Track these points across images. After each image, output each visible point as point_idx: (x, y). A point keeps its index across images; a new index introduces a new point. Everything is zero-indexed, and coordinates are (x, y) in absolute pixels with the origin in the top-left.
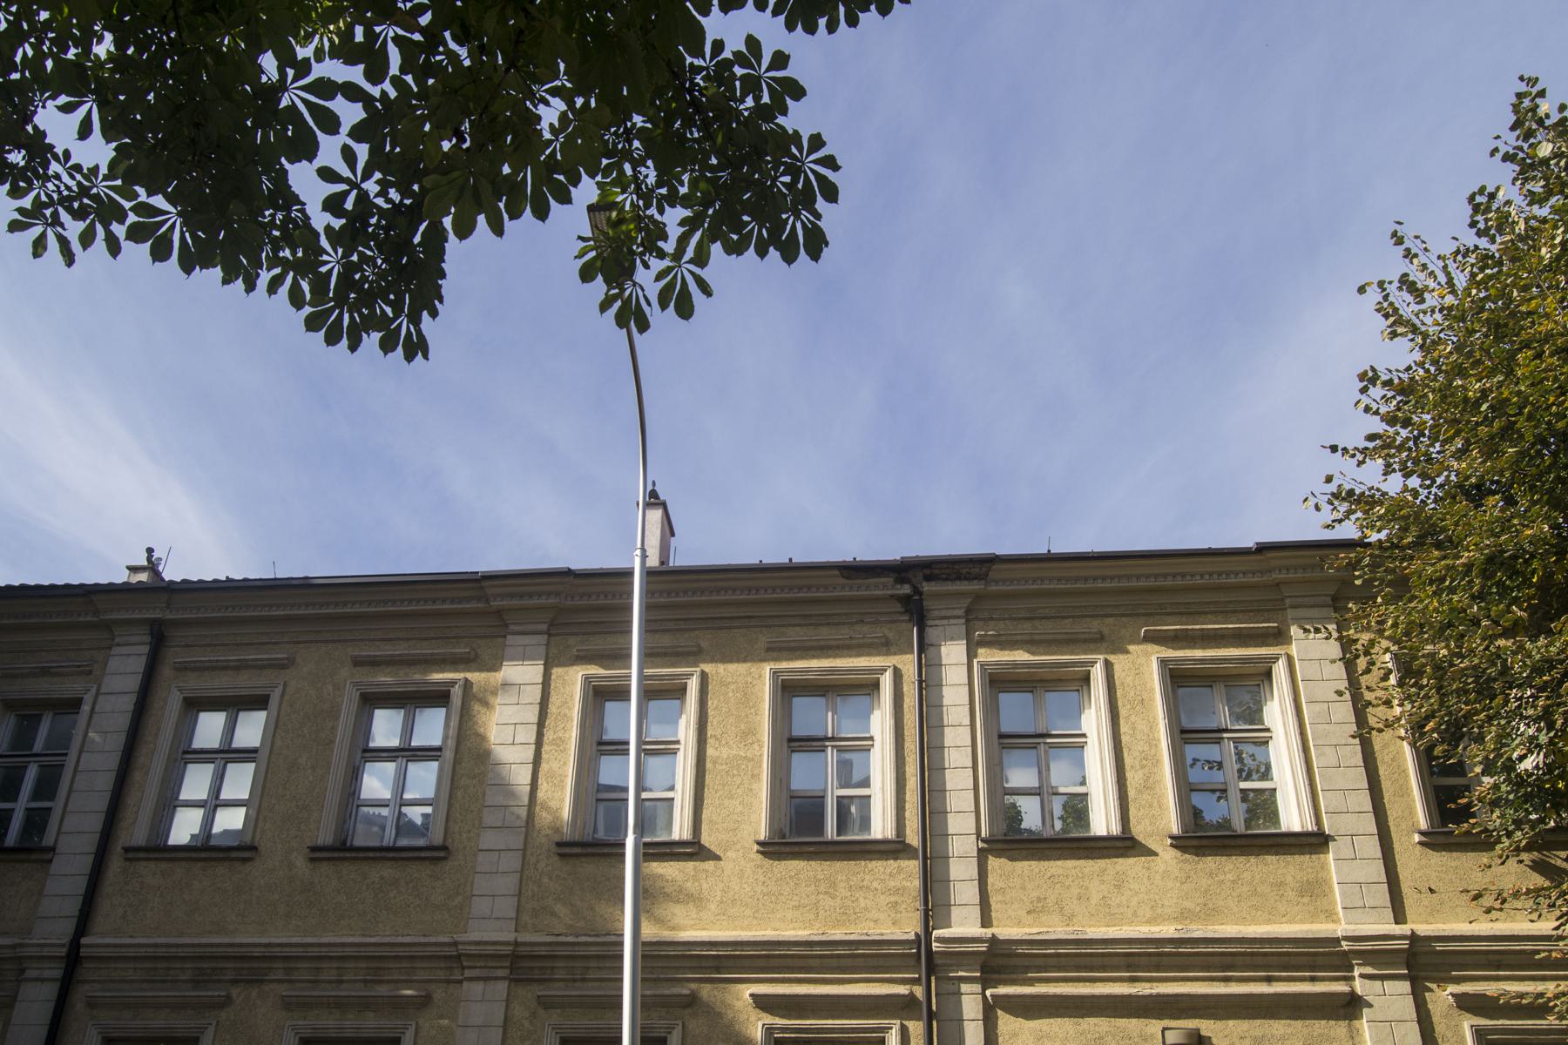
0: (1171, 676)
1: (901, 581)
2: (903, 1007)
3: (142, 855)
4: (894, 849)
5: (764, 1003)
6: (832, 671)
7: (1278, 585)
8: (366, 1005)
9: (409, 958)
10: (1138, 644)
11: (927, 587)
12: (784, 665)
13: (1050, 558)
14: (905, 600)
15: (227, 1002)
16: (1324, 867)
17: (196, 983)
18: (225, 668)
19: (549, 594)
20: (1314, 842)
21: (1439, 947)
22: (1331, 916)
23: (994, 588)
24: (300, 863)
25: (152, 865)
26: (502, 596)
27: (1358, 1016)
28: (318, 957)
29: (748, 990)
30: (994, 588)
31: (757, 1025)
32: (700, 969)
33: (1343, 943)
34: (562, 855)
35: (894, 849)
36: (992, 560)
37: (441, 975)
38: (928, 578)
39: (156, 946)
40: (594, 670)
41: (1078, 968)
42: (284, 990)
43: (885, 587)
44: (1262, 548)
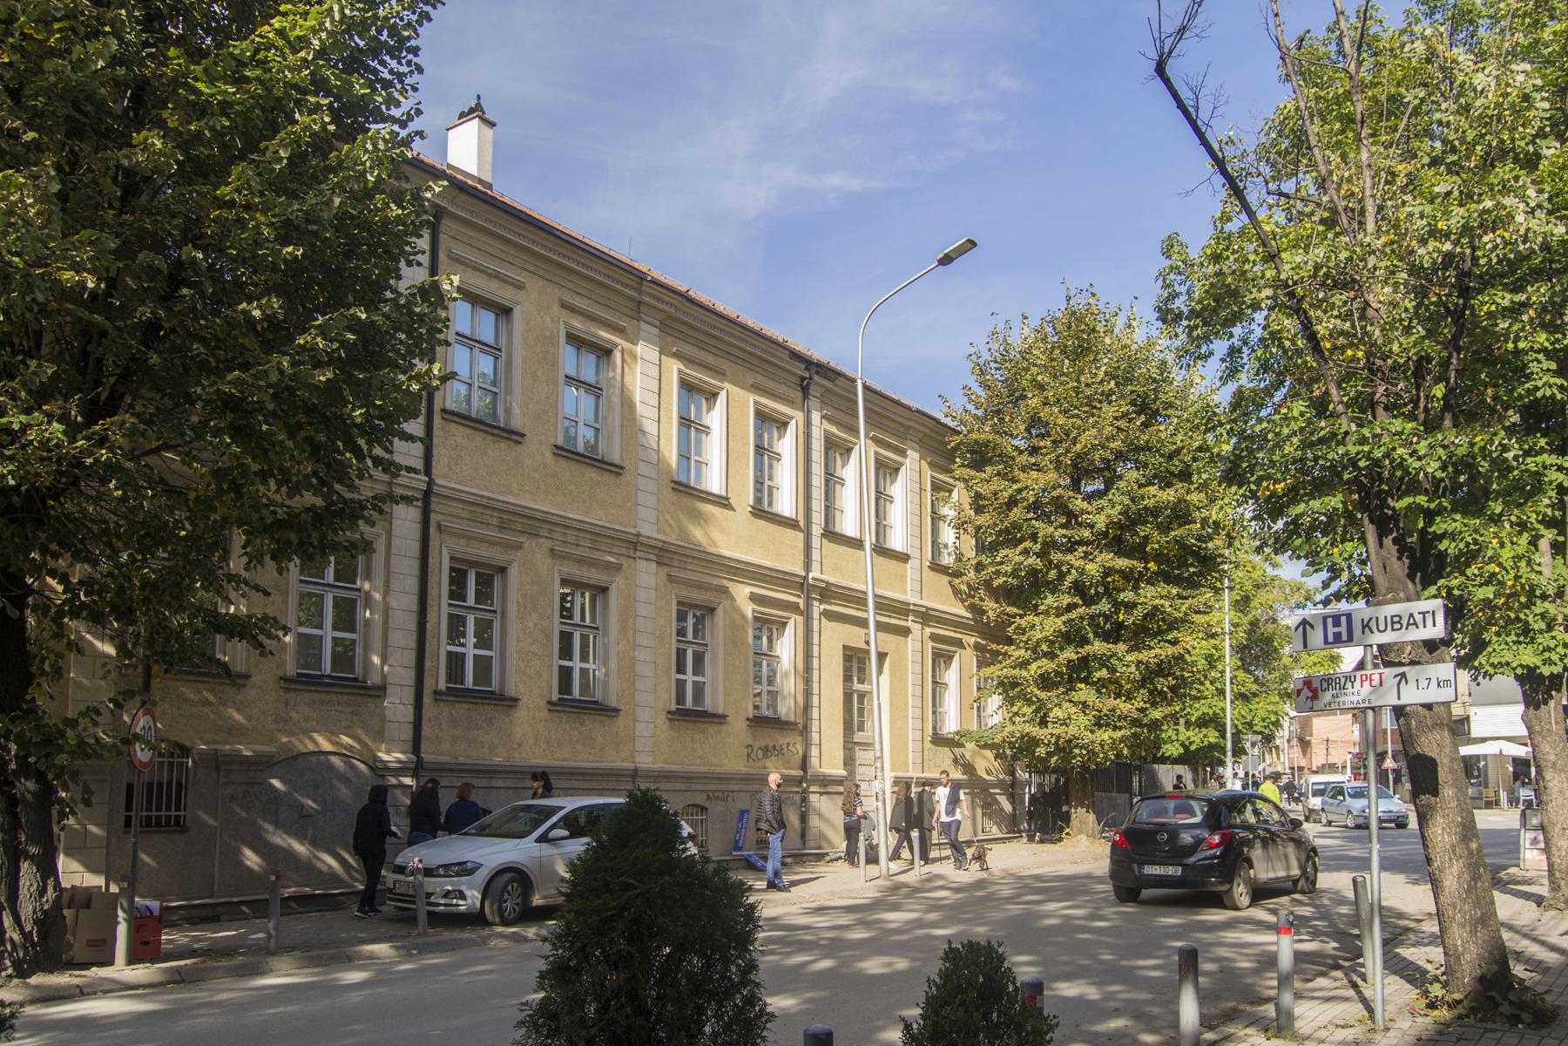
0: (826, 441)
1: (807, 369)
2: (794, 608)
3: (456, 419)
4: (791, 524)
5: (754, 598)
6: (775, 410)
7: (909, 427)
8: (593, 563)
9: (598, 535)
10: (742, 387)
11: (816, 378)
12: (941, 477)
13: (685, 297)
14: (803, 379)
15: (519, 547)
16: (906, 570)
17: (501, 528)
18: (482, 272)
19: (671, 305)
20: (903, 558)
21: (833, 589)
22: (905, 592)
23: (835, 389)
24: (548, 453)
25: (460, 427)
26: (650, 295)
27: (907, 636)
28: (579, 528)
29: (748, 590)
30: (835, 389)
31: (749, 609)
32: (727, 573)
33: (495, 522)
34: (555, 454)
35: (791, 524)
36: (839, 374)
37: (624, 551)
38: (817, 373)
39: (482, 496)
40: (833, 429)
41: (760, 580)
42: (548, 543)
43: (799, 369)
44: (918, 411)
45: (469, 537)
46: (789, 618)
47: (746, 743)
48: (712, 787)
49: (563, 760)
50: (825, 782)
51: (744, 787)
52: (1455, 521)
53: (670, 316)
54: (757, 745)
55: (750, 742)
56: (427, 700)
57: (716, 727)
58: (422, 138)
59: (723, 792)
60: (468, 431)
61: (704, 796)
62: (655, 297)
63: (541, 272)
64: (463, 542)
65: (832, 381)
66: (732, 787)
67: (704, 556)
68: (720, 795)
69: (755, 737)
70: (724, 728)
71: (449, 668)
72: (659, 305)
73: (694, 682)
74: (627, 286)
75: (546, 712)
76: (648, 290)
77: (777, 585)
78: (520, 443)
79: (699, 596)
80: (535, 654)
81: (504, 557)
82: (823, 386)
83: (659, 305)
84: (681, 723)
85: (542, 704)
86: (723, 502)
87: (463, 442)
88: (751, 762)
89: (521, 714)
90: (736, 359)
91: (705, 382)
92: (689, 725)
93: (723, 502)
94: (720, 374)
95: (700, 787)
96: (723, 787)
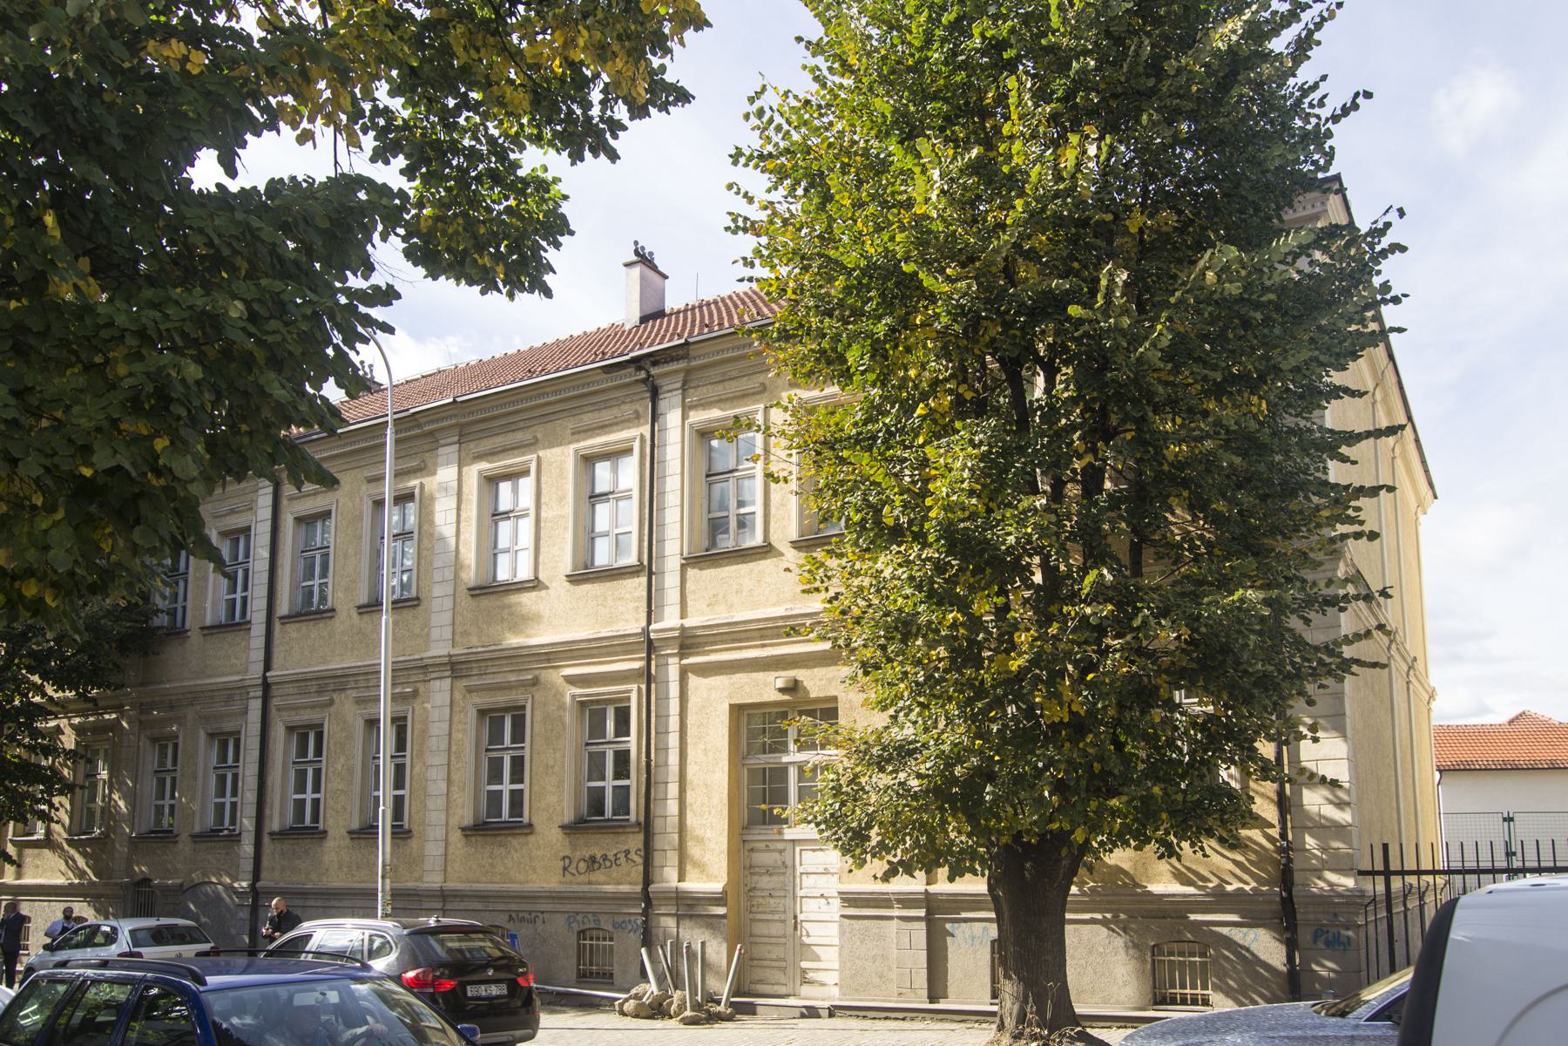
1: (639, 369)
6: (606, 444)
11: (654, 371)
14: (644, 381)
23: (694, 363)
24: (354, 613)
26: (428, 423)
30: (694, 363)
38: (655, 364)
42: (353, 693)
43: (630, 375)
45: (296, 708)
46: (629, 691)
47: (562, 854)
48: (513, 907)
49: (363, 882)
50: (689, 907)
51: (558, 907)
52: (859, 60)
53: (462, 426)
54: (578, 855)
55: (567, 853)
56: (266, 839)
57: (522, 839)
58: (727, 229)
59: (530, 913)
60: (297, 625)
61: (505, 917)
62: (433, 422)
63: (354, 465)
64: (293, 713)
65: (686, 357)
66: (543, 907)
67: (511, 653)
68: (526, 916)
69: (574, 847)
70: (531, 839)
71: (522, 771)
72: (445, 423)
73: (603, 779)
74: (409, 429)
75: (348, 840)
76: (425, 420)
77: (609, 655)
78: (331, 617)
79: (501, 699)
80: (342, 791)
81: (319, 716)
82: (676, 372)
83: (445, 423)
84: (479, 839)
85: (343, 832)
86: (535, 584)
87: (294, 635)
88: (568, 876)
89: (330, 844)
90: (546, 418)
91: (510, 466)
92: (488, 839)
93: (535, 584)
94: (532, 445)
95: (500, 907)
96: (528, 907)
